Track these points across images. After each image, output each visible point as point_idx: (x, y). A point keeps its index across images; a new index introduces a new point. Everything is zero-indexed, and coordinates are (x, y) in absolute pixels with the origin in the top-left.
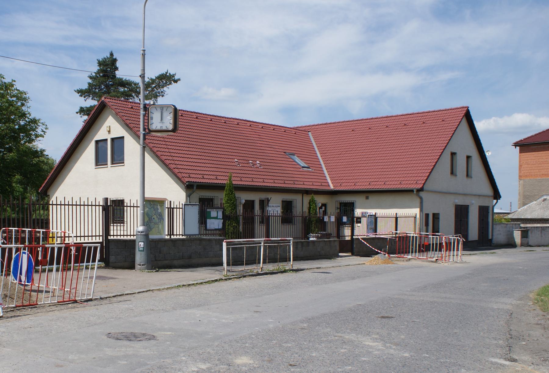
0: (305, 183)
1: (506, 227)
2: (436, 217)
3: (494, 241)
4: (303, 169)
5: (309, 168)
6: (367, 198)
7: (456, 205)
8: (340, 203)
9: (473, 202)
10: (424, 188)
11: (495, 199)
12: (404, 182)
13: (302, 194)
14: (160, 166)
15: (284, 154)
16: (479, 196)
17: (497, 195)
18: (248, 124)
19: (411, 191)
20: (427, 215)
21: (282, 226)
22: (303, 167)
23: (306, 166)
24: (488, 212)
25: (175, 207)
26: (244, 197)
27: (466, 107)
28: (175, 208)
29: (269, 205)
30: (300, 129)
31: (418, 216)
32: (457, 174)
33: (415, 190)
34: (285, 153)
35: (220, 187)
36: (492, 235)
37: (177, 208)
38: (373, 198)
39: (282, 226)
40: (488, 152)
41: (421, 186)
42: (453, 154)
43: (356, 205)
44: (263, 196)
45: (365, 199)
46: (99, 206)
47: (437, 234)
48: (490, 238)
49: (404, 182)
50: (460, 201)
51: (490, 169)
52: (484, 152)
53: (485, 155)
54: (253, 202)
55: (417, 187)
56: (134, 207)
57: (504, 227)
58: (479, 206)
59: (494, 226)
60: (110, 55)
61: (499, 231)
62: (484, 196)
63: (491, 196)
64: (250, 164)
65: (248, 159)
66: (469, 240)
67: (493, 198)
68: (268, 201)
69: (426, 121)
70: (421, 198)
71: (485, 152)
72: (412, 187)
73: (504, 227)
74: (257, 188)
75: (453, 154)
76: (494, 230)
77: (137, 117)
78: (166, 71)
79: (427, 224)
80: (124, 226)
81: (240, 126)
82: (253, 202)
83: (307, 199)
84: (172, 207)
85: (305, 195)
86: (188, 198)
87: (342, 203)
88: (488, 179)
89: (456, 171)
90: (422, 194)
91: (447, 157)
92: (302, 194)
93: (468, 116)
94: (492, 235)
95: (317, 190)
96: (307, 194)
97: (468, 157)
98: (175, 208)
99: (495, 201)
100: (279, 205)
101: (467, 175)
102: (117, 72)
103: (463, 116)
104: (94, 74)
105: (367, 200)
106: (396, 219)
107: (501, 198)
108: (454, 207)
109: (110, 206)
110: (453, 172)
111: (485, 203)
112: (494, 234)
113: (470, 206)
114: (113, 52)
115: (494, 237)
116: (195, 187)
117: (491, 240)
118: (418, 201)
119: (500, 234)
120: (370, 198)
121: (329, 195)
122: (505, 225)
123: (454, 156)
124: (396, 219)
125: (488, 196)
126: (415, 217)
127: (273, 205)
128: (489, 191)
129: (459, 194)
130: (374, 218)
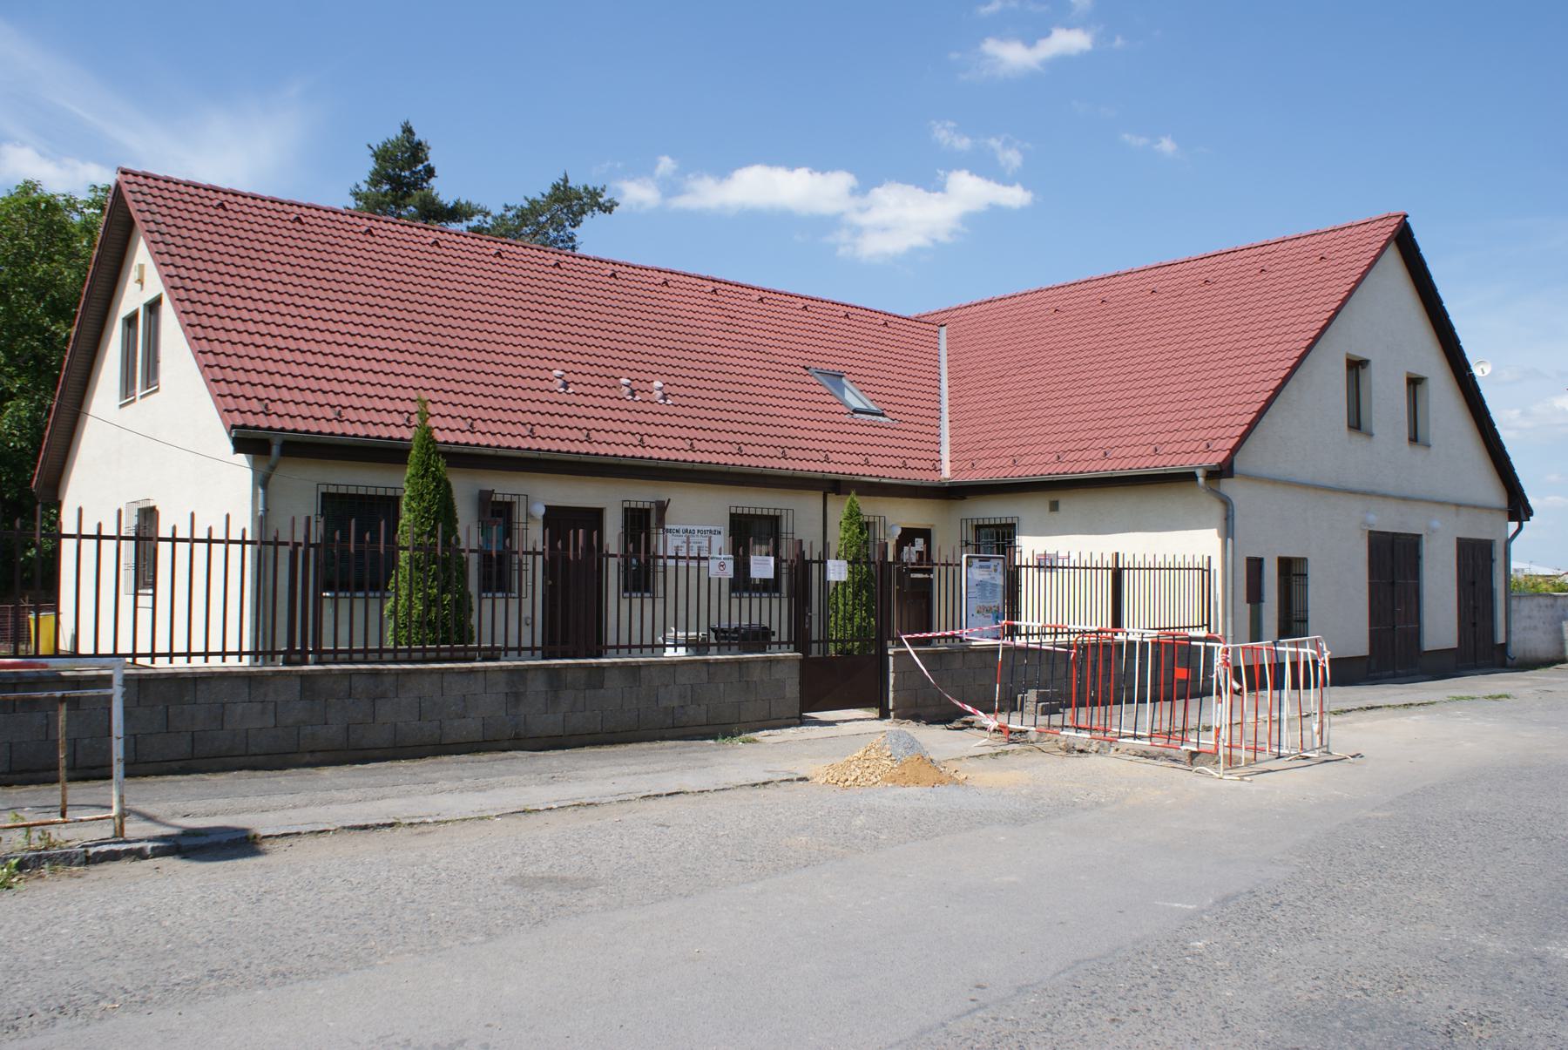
0: (872, 460)
1: (1552, 606)
2: (1292, 570)
3: (1515, 650)
4: (857, 415)
5: (883, 415)
6: (1054, 507)
7: (1370, 532)
8: (978, 527)
9: (1436, 524)
10: (1236, 466)
11: (1511, 519)
12: (1168, 448)
13: (821, 494)
14: (103, 359)
15: (805, 372)
16: (1458, 505)
17: (1518, 508)
18: (710, 287)
19: (1190, 477)
20: (1255, 566)
21: (735, 602)
22: (856, 411)
23: (873, 408)
24: (1492, 560)
25: (1024, 563)
26: (464, 488)
27: (1399, 216)
28: (815, 562)
29: (667, 527)
30: (925, 319)
31: (1217, 565)
32: (1375, 430)
33: (1200, 473)
34: (807, 369)
35: (389, 453)
36: (1508, 632)
37: (1027, 567)
38: (1072, 504)
39: (735, 602)
40: (1481, 366)
41: (1220, 457)
42: (1356, 366)
43: (1021, 527)
44: (642, 494)
45: (1048, 509)
46: (1107, 568)
47: (161, 844)
48: (1501, 639)
49: (1168, 448)
50: (1391, 520)
51: (1491, 424)
52: (1467, 367)
53: (1472, 377)
54: (594, 518)
55: (1209, 460)
56: (1097, 568)
57: (1547, 606)
58: (1458, 539)
59: (1514, 603)
60: (404, 132)
61: (1530, 617)
62: (1475, 507)
63: (1500, 510)
64: (624, 388)
65: (649, 377)
66: (1426, 649)
67: (1506, 516)
68: (662, 507)
69: (1271, 266)
70: (1226, 503)
71: (1472, 368)
72: (1191, 462)
73: (1547, 606)
74: (579, 463)
75: (1356, 366)
76: (1514, 617)
77: (932, 422)
78: (563, 177)
79: (1255, 594)
80: (780, 598)
81: (671, 290)
82: (594, 518)
83: (839, 509)
84: (1121, 566)
85: (831, 498)
86: (260, 491)
87: (987, 526)
88: (1471, 418)
89: (1370, 420)
90: (1227, 486)
91: (1328, 374)
92: (821, 494)
93: (1403, 239)
94: (1508, 632)
95: (877, 480)
96: (838, 493)
97: (1414, 382)
98: (815, 562)
99: (1513, 526)
100: (718, 528)
101: (1414, 439)
102: (432, 181)
103: (1388, 241)
104: (364, 187)
105: (1054, 514)
106: (1117, 575)
107: (1532, 515)
108: (1366, 540)
109: (894, 563)
110: (1356, 423)
111: (1479, 529)
112: (1514, 627)
113: (1424, 538)
114: (411, 124)
115: (1514, 638)
116: (275, 450)
117: (1504, 646)
118: (1217, 510)
119: (1535, 628)
120: (1062, 506)
121: (937, 501)
122: (1549, 601)
123: (1361, 372)
124: (1117, 575)
125: (1490, 509)
126: (1206, 571)
127: (689, 528)
128: (1494, 494)
129: (1385, 496)
130: (1000, 569)
